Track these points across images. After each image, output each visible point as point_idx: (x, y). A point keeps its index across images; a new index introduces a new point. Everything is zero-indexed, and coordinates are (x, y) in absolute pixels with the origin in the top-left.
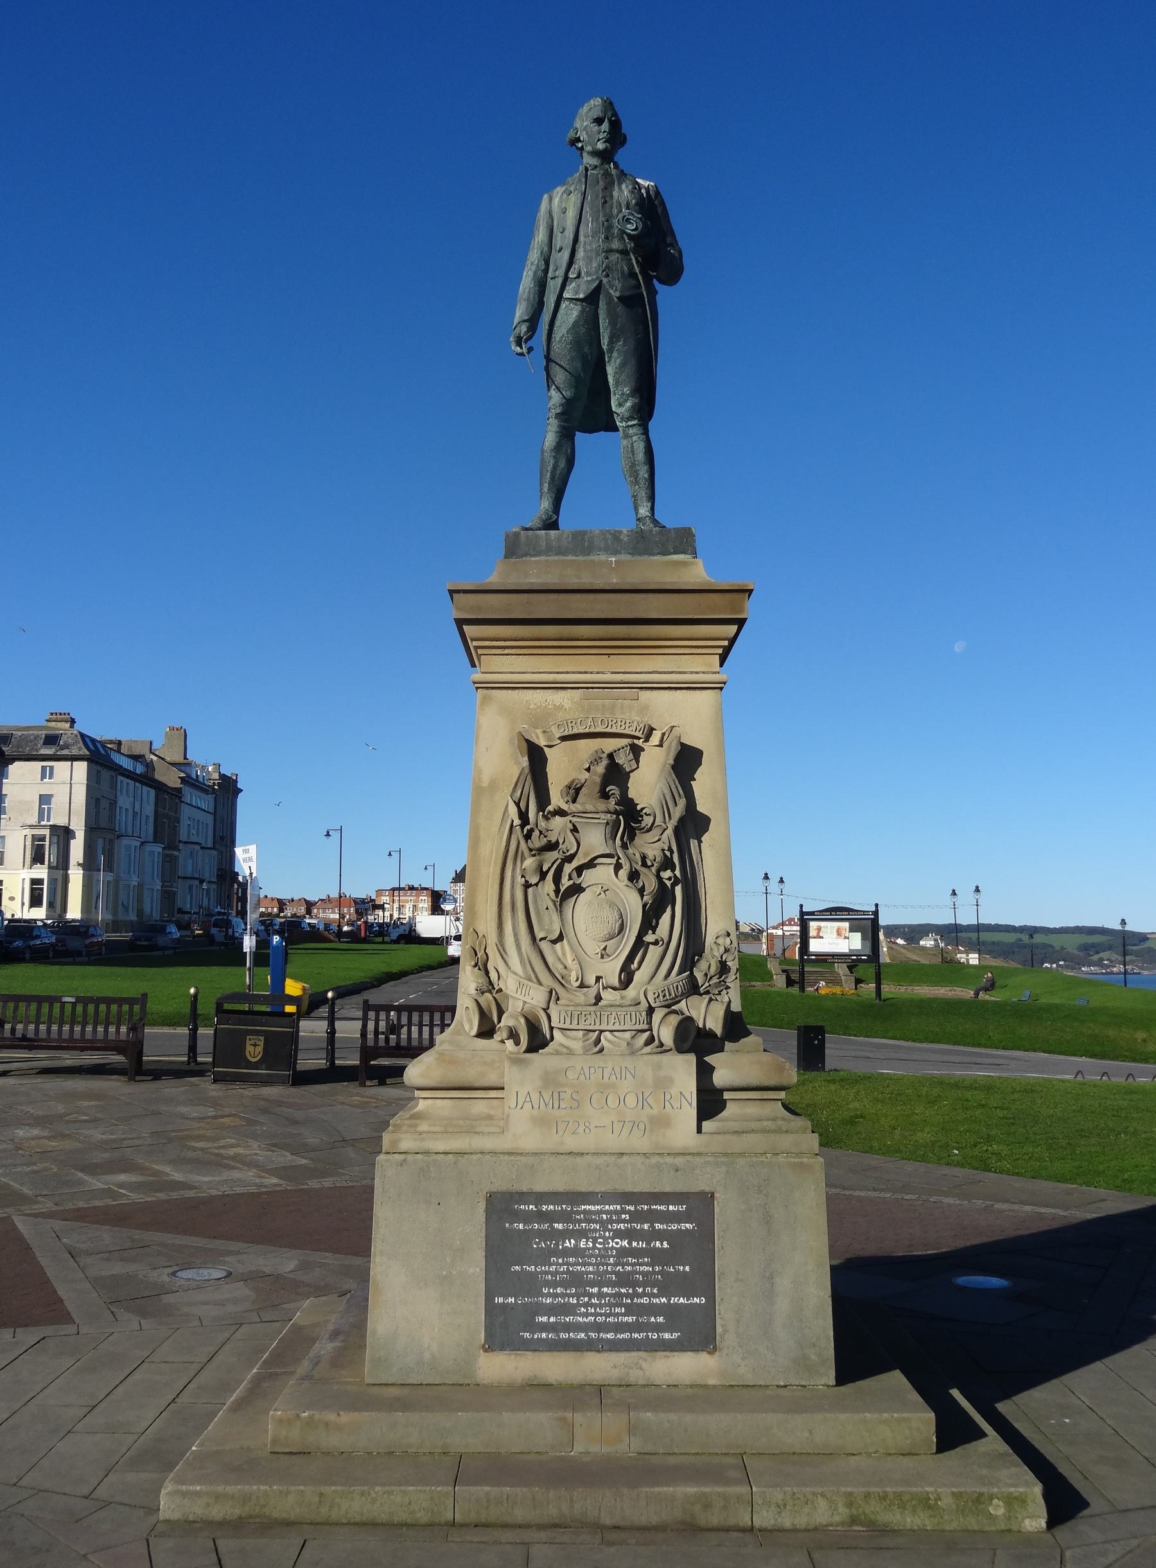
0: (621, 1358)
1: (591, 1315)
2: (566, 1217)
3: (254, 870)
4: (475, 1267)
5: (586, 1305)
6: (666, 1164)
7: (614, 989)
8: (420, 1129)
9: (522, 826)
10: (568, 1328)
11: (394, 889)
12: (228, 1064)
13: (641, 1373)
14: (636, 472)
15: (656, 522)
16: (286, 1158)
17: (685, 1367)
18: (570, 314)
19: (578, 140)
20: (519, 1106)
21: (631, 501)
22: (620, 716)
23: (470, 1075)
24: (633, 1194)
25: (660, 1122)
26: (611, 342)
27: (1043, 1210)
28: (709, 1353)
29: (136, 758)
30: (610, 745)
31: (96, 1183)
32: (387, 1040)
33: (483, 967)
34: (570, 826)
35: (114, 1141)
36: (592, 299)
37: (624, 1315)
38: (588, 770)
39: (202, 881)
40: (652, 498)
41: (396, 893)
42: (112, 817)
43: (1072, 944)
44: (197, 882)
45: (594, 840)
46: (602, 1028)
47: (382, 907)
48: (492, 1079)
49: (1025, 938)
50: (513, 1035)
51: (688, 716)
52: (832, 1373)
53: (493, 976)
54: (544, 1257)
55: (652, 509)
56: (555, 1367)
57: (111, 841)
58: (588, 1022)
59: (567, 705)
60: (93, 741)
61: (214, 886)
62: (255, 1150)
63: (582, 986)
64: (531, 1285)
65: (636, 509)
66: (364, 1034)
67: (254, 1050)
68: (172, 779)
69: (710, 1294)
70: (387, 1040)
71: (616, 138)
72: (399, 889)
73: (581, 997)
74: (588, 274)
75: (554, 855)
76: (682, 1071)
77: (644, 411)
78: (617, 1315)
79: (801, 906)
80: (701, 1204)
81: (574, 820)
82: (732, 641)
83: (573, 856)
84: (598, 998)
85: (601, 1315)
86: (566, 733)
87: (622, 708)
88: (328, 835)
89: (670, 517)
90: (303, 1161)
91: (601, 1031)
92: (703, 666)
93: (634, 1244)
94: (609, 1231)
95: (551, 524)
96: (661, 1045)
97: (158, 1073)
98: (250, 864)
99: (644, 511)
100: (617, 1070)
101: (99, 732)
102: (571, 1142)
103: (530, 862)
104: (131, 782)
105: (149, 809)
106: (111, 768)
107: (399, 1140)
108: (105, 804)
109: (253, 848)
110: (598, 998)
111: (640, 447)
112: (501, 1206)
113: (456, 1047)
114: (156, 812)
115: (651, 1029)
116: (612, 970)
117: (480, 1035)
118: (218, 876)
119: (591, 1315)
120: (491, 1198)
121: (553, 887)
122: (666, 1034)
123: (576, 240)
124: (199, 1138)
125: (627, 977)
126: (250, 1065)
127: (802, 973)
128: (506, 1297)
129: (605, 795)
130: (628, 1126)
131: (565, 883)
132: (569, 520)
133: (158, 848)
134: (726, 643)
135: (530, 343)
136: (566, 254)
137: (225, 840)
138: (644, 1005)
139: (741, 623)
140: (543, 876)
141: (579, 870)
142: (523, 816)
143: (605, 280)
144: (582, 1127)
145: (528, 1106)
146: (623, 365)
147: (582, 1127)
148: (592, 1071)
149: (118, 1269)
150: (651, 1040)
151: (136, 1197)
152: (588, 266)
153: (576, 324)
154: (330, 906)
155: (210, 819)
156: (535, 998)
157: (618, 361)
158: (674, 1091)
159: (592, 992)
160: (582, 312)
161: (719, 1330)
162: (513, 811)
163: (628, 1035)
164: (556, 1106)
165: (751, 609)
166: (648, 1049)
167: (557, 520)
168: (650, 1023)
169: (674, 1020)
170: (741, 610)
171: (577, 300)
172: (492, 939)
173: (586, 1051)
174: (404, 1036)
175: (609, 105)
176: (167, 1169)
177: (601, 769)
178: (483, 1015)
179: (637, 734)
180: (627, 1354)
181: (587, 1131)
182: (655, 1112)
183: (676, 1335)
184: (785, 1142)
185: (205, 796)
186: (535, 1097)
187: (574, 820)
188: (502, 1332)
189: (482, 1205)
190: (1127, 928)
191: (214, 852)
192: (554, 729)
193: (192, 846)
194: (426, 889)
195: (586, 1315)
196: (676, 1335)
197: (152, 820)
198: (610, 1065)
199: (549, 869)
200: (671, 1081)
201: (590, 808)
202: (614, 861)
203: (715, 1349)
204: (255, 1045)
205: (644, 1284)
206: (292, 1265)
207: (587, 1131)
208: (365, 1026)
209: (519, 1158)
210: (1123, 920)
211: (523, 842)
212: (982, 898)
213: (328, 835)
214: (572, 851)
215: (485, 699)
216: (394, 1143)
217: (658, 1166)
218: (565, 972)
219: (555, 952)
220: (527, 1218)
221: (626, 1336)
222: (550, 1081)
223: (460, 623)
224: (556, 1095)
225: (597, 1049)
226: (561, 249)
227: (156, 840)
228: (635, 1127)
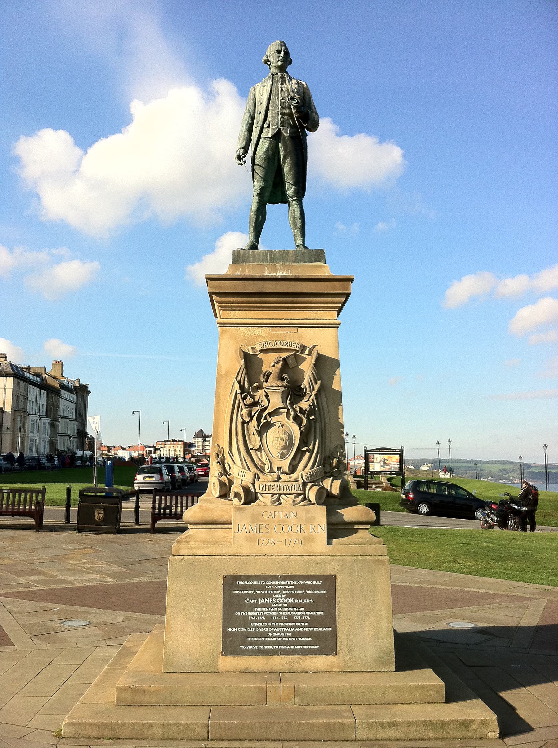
0: (290, 658)
1: (275, 637)
2: (263, 588)
3: (97, 428)
4: (218, 613)
5: (273, 632)
7: (288, 474)
8: (190, 543)
9: (241, 394)
10: (264, 643)
11: (165, 442)
12: (86, 524)
13: (299, 666)
14: (296, 222)
15: (306, 248)
16: (114, 568)
17: (321, 661)
18: (264, 145)
19: (269, 61)
20: (240, 532)
22: (289, 341)
23: (216, 515)
24: (296, 576)
25: (309, 540)
26: (285, 158)
27: (490, 591)
28: (333, 655)
29: (38, 375)
30: (284, 355)
31: (22, 580)
33: (222, 462)
34: (265, 394)
35: (31, 560)
36: (277, 136)
37: (292, 637)
38: (273, 366)
39: (70, 438)
40: (303, 235)
41: (166, 443)
42: (25, 404)
43: (496, 469)
44: (68, 438)
45: (276, 401)
46: (280, 492)
47: (158, 449)
48: (226, 518)
49: (472, 465)
50: (237, 495)
51: (322, 341)
52: (394, 665)
53: (227, 466)
54: (252, 607)
55: (304, 241)
56: (257, 663)
57: (24, 417)
58: (274, 490)
59: (263, 334)
60: (17, 367)
61: (76, 440)
62: (101, 565)
63: (271, 472)
64: (246, 622)
65: (296, 241)
66: (153, 508)
67: (99, 516)
68: (56, 384)
69: (334, 624)
71: (287, 60)
72: (168, 441)
73: (270, 477)
74: (273, 126)
75: (259, 408)
76: (320, 514)
77: (300, 192)
78: (288, 637)
80: (329, 581)
81: (266, 390)
82: (344, 304)
83: (266, 408)
84: (279, 478)
85: (280, 637)
86: (263, 348)
88: (133, 414)
89: (312, 244)
90: (125, 570)
91: (280, 495)
92: (329, 316)
93: (296, 601)
94: (284, 594)
95: (254, 247)
96: (310, 501)
97: (52, 529)
98: (96, 425)
99: (299, 242)
100: (288, 513)
102: (265, 550)
103: (245, 411)
104: (35, 388)
105: (44, 401)
106: (25, 381)
107: (180, 549)
109: (97, 417)
110: (279, 478)
111: (297, 210)
112: (231, 582)
113: (208, 504)
114: (47, 402)
115: (304, 494)
116: (285, 464)
117: (220, 497)
118: (78, 433)
119: (275, 637)
120: (226, 578)
121: (256, 423)
122: (312, 495)
123: (267, 109)
124: (73, 559)
125: (293, 468)
127: (366, 482)
128: (233, 628)
129: (282, 379)
130: (293, 541)
131: (263, 421)
132: (261, 247)
133: (48, 421)
134: (340, 305)
135: (244, 160)
136: (263, 115)
137: (81, 416)
138: (301, 481)
139: (348, 295)
141: (270, 414)
142: (242, 387)
143: (281, 128)
144: (271, 542)
146: (290, 169)
148: (276, 513)
149: (33, 620)
150: (304, 499)
151: (40, 587)
152: (274, 118)
153: (267, 150)
154: (133, 449)
155: (74, 406)
156: (248, 479)
157: (288, 168)
158: (316, 524)
159: (275, 476)
160: (270, 144)
162: (237, 386)
163: (293, 496)
164: (258, 532)
165: (353, 288)
166: (303, 503)
167: (257, 246)
168: (305, 490)
169: (316, 488)
170: (348, 289)
171: (268, 137)
172: (226, 449)
173: (273, 503)
174: (173, 510)
175: (283, 43)
176: (56, 574)
177: (279, 365)
178: (222, 484)
179: (298, 349)
180: (293, 656)
182: (306, 534)
183: (317, 647)
184: (370, 549)
185: (72, 395)
186: (247, 527)
187: (266, 390)
188: (232, 645)
189: (222, 582)
191: (76, 423)
192: (257, 346)
193: (66, 420)
194: (181, 441)
195: (273, 637)
196: (317, 647)
197: (45, 406)
198: (284, 511)
199: (255, 414)
200: (314, 519)
201: (274, 384)
202: (286, 410)
203: (336, 653)
206: (121, 619)
208: (154, 503)
209: (239, 557)
210: (521, 456)
211: (241, 402)
213: (133, 414)
214: (266, 406)
215: (223, 332)
216: (178, 550)
217: (308, 561)
218: (262, 465)
219: (257, 455)
220: (244, 588)
221: (292, 647)
222: (255, 519)
223: (211, 294)
224: (258, 526)
225: (277, 503)
226: (260, 113)
227: (47, 416)
228: (297, 542)
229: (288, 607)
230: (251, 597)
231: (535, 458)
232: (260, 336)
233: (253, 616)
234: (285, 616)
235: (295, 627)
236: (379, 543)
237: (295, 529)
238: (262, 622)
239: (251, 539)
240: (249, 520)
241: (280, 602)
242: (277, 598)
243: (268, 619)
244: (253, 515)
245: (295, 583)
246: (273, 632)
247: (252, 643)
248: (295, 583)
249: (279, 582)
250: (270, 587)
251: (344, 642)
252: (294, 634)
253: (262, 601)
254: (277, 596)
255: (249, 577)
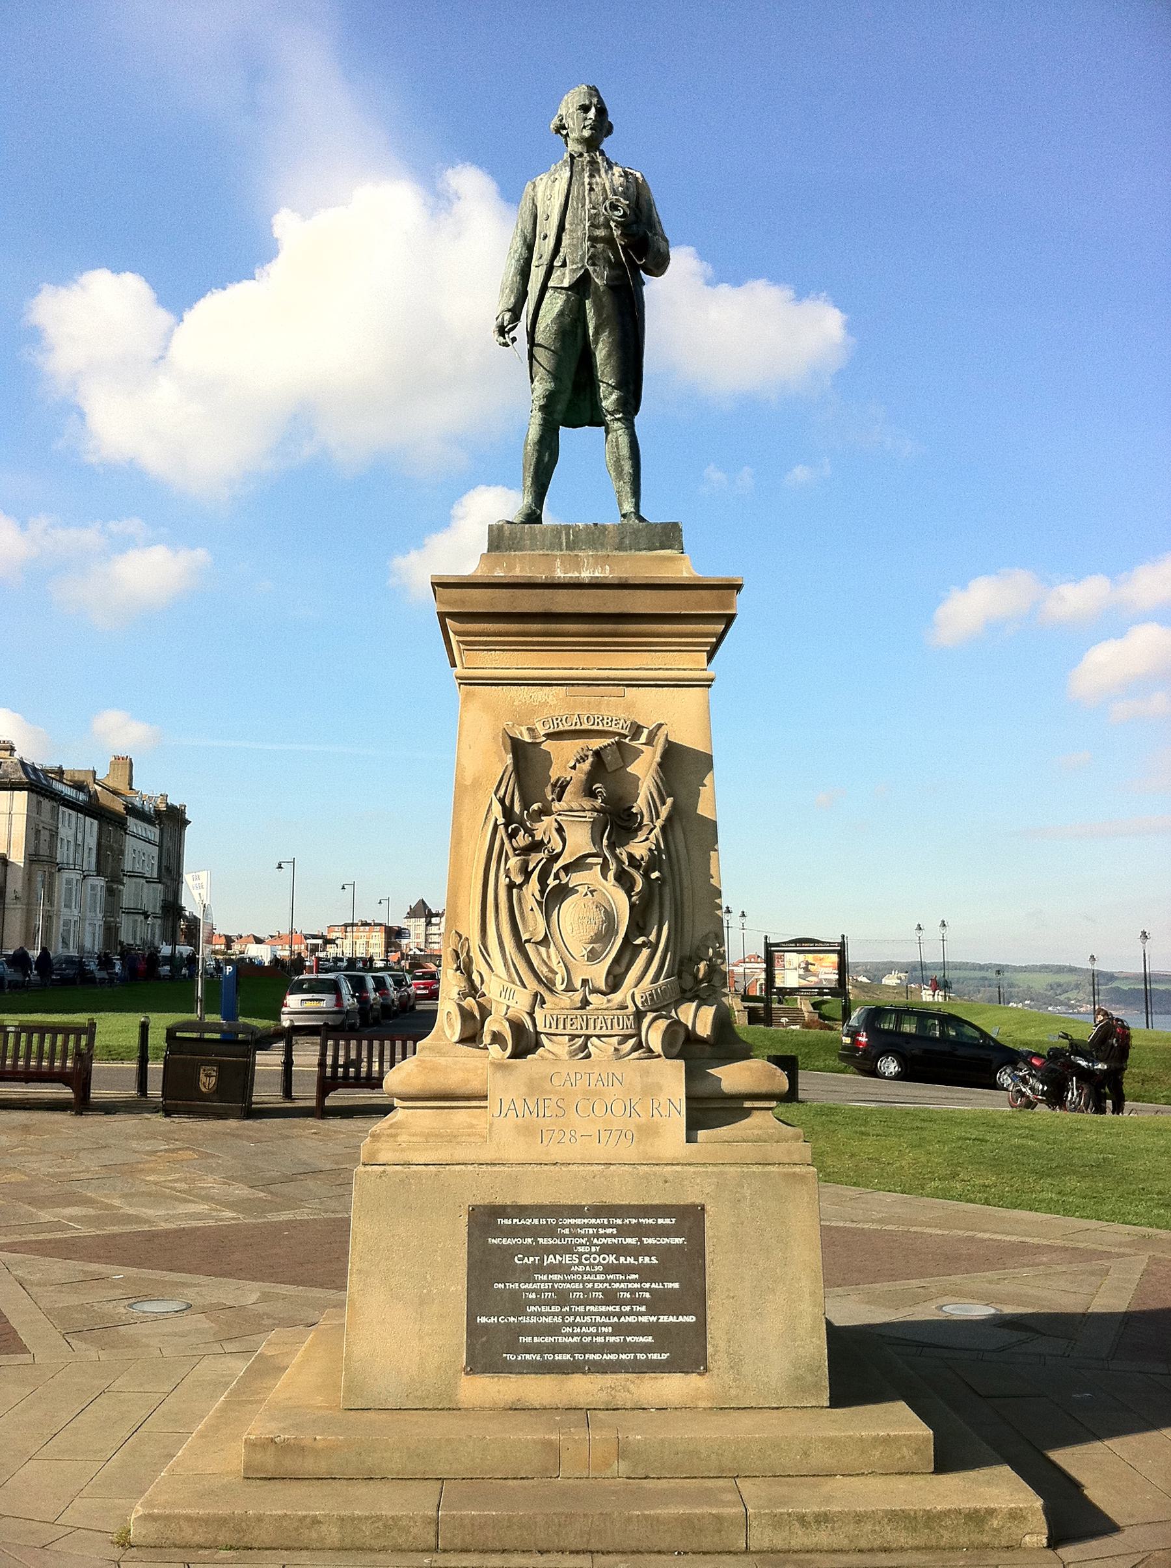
0: (609, 1379)
1: (577, 1335)
2: (551, 1232)
3: (204, 897)
4: (458, 1286)
5: (573, 1325)
6: (655, 1174)
8: (399, 1139)
9: (506, 825)
10: (555, 1349)
11: (346, 926)
12: (180, 1098)
13: (628, 1395)
14: (621, 466)
15: (641, 519)
16: (240, 1191)
17: (673, 1387)
18: (554, 304)
19: (564, 128)
20: (503, 1114)
21: (615, 498)
22: (606, 714)
23: (453, 1080)
24: (621, 1207)
25: (648, 1131)
26: (597, 332)
27: (1027, 1239)
28: (699, 1374)
29: (79, 786)
30: (597, 744)
31: (46, 1215)
32: (346, 1072)
33: (466, 969)
34: (555, 825)
35: (64, 1174)
36: (582, 286)
37: (612, 1335)
38: (574, 767)
39: (147, 917)
40: (636, 493)
41: (349, 929)
42: (52, 846)
43: (1040, 983)
45: (579, 840)
46: (588, 1032)
47: (332, 942)
48: (474, 1086)
49: (991, 974)
50: (497, 1038)
51: (676, 716)
52: (826, 1395)
53: (475, 977)
54: (528, 1273)
55: (637, 505)
56: (539, 1389)
57: (51, 875)
58: (574, 1027)
59: (552, 701)
60: (35, 770)
61: (159, 921)
62: (212, 1183)
63: (570, 989)
64: (517, 1304)
65: (620, 505)
66: (322, 1064)
67: (207, 1081)
70: (346, 1072)
71: (602, 126)
72: (353, 925)
73: (566, 1000)
74: (573, 263)
75: (543, 855)
76: (671, 1078)
77: (630, 403)
78: (605, 1335)
79: (766, 937)
80: (691, 1218)
81: (559, 818)
82: (721, 637)
83: (559, 855)
84: (585, 1003)
85: (587, 1335)
86: (551, 730)
87: (608, 704)
88: (280, 867)
89: (654, 512)
90: (262, 1194)
91: (588, 1037)
92: (690, 663)
93: (622, 1259)
94: (596, 1245)
95: (533, 517)
96: (651, 1051)
97: (109, 1108)
99: (628, 507)
100: (604, 1076)
101: (43, 759)
102: (557, 1153)
103: (514, 862)
104: (73, 813)
105: (92, 841)
106: (53, 799)
107: (378, 1151)
108: (45, 835)
109: (203, 875)
110: (585, 1003)
111: (624, 441)
112: (485, 1219)
113: (437, 1057)
114: (99, 844)
115: (639, 1035)
116: (598, 973)
119: (577, 1335)
120: (474, 1212)
121: (538, 887)
122: (655, 1038)
123: (561, 228)
124: (153, 1171)
125: (615, 982)
126: (203, 1097)
127: (768, 1009)
128: (488, 1316)
129: (592, 794)
131: (552, 882)
132: (547, 518)
133: (100, 882)
134: (714, 640)
135: (512, 334)
136: (551, 241)
137: (170, 873)
138: (632, 1009)
139: (729, 619)
140: (527, 875)
141: (567, 868)
142: (508, 812)
143: (591, 269)
144: (568, 1136)
145: (512, 1113)
146: (609, 355)
147: (568, 1136)
148: (578, 1076)
150: (639, 1046)
152: (575, 248)
153: (561, 314)
155: (155, 851)
156: (520, 1003)
157: (604, 352)
158: (663, 1099)
159: (578, 997)
160: (567, 301)
161: (710, 1350)
162: (497, 809)
163: (615, 1040)
164: (541, 1114)
165: (741, 604)
166: (635, 1055)
167: (540, 515)
168: (639, 1028)
169: (662, 1024)
170: (730, 606)
171: (562, 288)
172: (475, 942)
173: (573, 1054)
174: (364, 1070)
175: (594, 91)
176: (117, 1202)
177: (586, 766)
178: (466, 1015)
179: (625, 732)
181: (573, 1140)
182: (643, 1120)
183: (665, 1356)
184: (777, 1151)
186: (519, 1104)
187: (559, 818)
188: (486, 1353)
189: (465, 1219)
190: (1097, 967)
191: (160, 886)
193: (138, 880)
194: (380, 925)
195: (572, 1335)
196: (665, 1356)
197: (94, 852)
198: (596, 1071)
199: (535, 868)
201: (575, 806)
202: (600, 860)
203: (706, 1369)
204: (209, 1076)
205: (632, 1302)
206: (254, 1297)
207: (573, 1140)
209: (502, 1168)
210: (1092, 957)
211: (506, 842)
212: (948, 932)
213: (280, 867)
215: (467, 697)
216: (373, 1154)
217: (646, 1176)
218: (550, 975)
219: (539, 954)
220: (512, 1232)
221: (613, 1357)
222: (534, 1087)
223: (442, 616)
224: (541, 1103)
225: (582, 1055)
226: (545, 237)
227: (99, 873)
228: (623, 1136)
229: (605, 1272)
230: (528, 1251)
231: (1123, 961)
232: (545, 704)
233: (530, 1291)
234: (597, 1291)
235: (619, 1315)
236: (796, 1138)
237: (618, 1108)
238: (549, 1303)
239: (526, 1131)
240: (523, 1089)
241: (587, 1262)
242: (580, 1254)
243: (562, 1298)
244: (531, 1080)
245: (619, 1221)
246: (573, 1325)
247: (528, 1349)
248: (619, 1221)
249: (586, 1221)
250: (567, 1231)
251: (722, 1345)
252: (618, 1329)
253: (550, 1260)
254: (580, 1249)
255: (522, 1211)
